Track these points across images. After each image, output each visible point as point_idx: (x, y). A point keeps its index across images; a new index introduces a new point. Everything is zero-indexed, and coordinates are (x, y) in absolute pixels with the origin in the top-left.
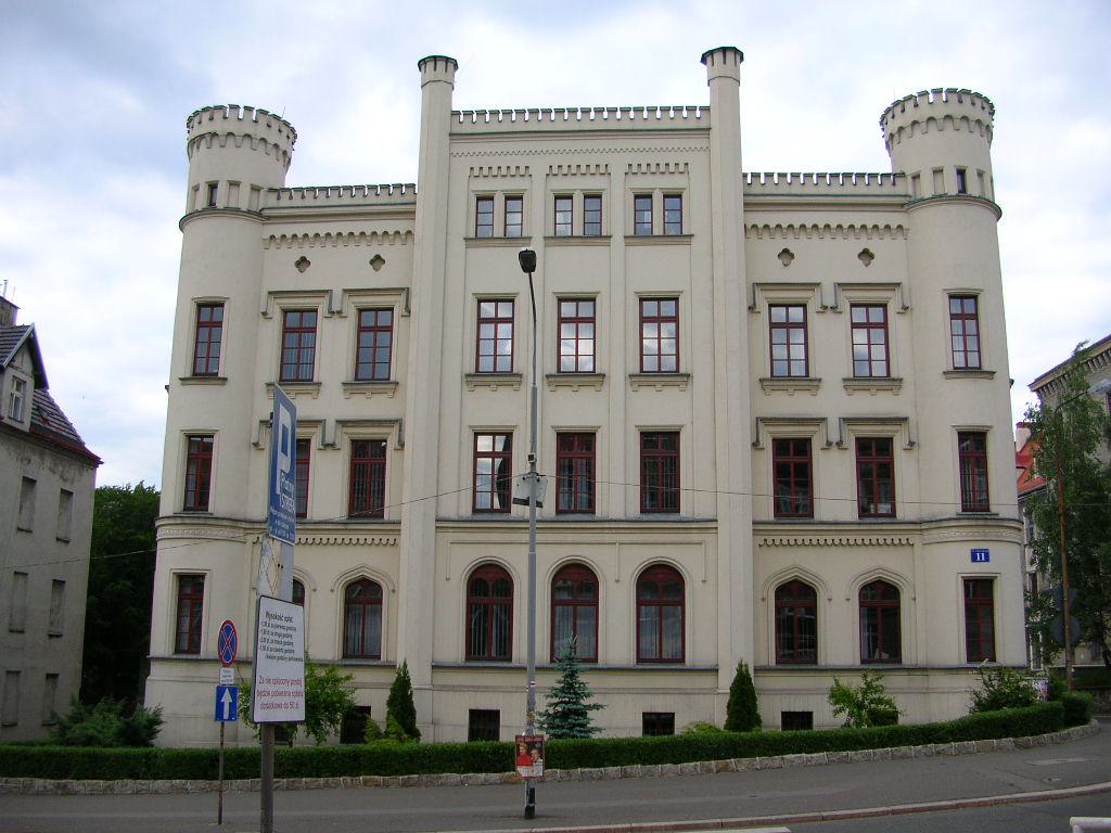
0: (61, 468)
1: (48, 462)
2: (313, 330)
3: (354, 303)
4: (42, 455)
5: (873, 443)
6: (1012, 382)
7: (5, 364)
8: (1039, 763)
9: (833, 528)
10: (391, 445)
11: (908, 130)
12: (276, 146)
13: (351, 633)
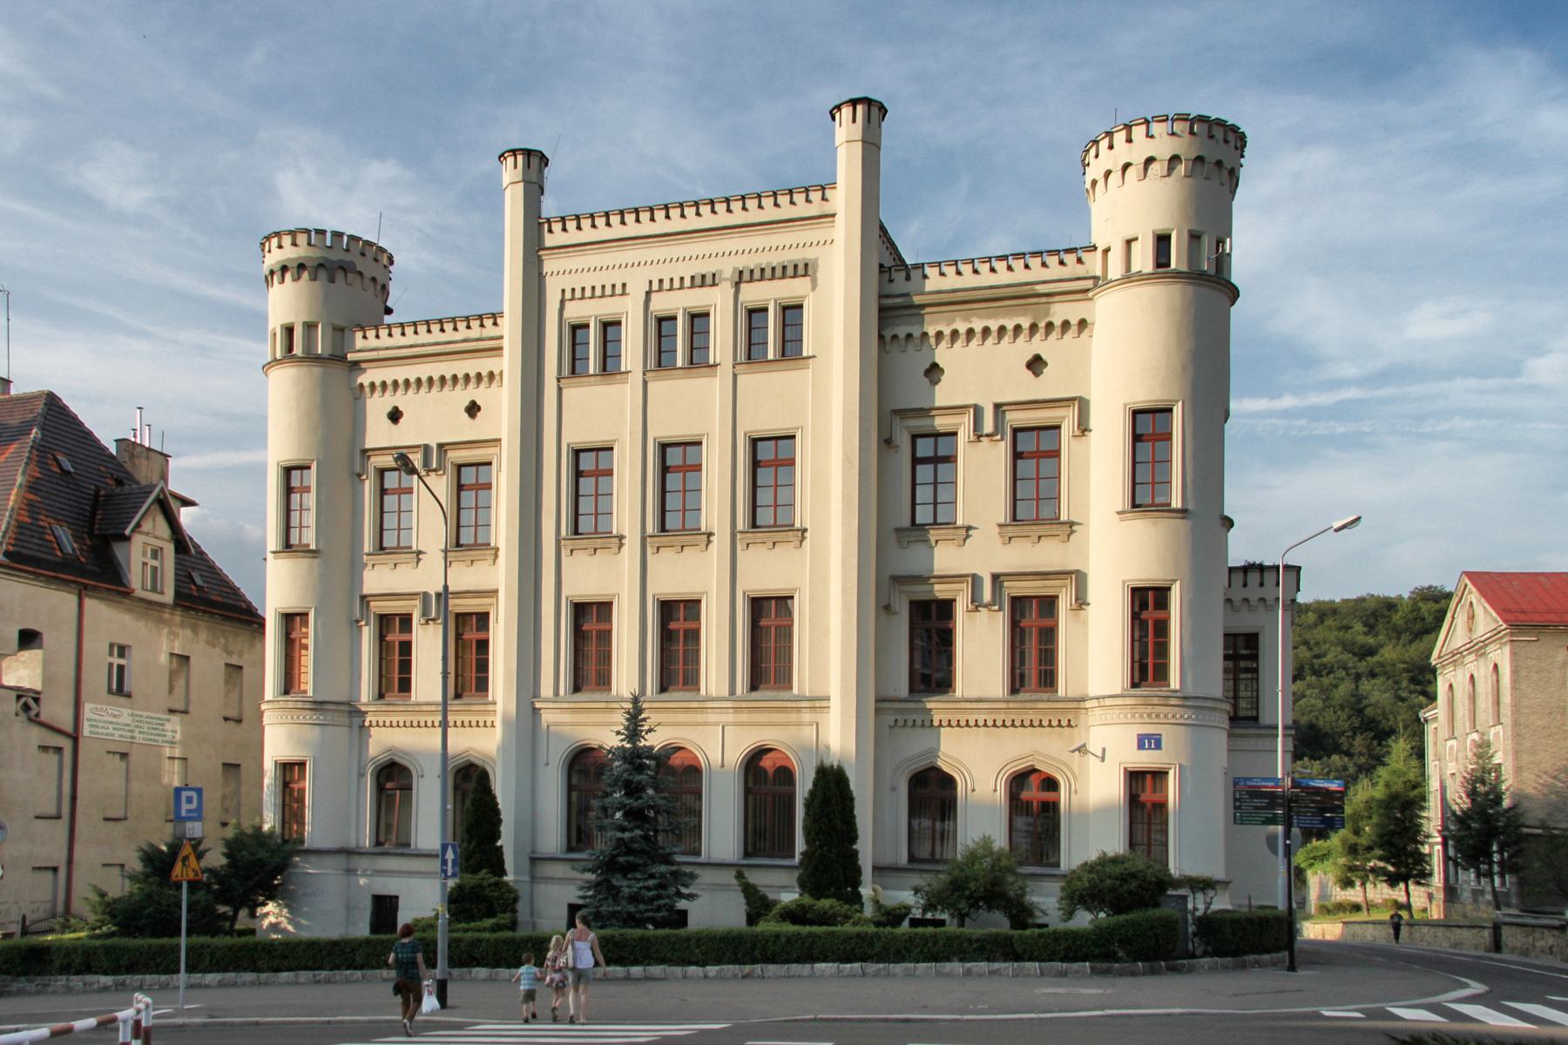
0: (222, 641)
1: (203, 635)
2: (1056, 454)
3: (907, 428)
4: (195, 629)
5: (934, 607)
7: (127, 532)
8: (1037, 991)
9: (975, 705)
10: (1064, 605)
12: (374, 280)
13: (916, 826)
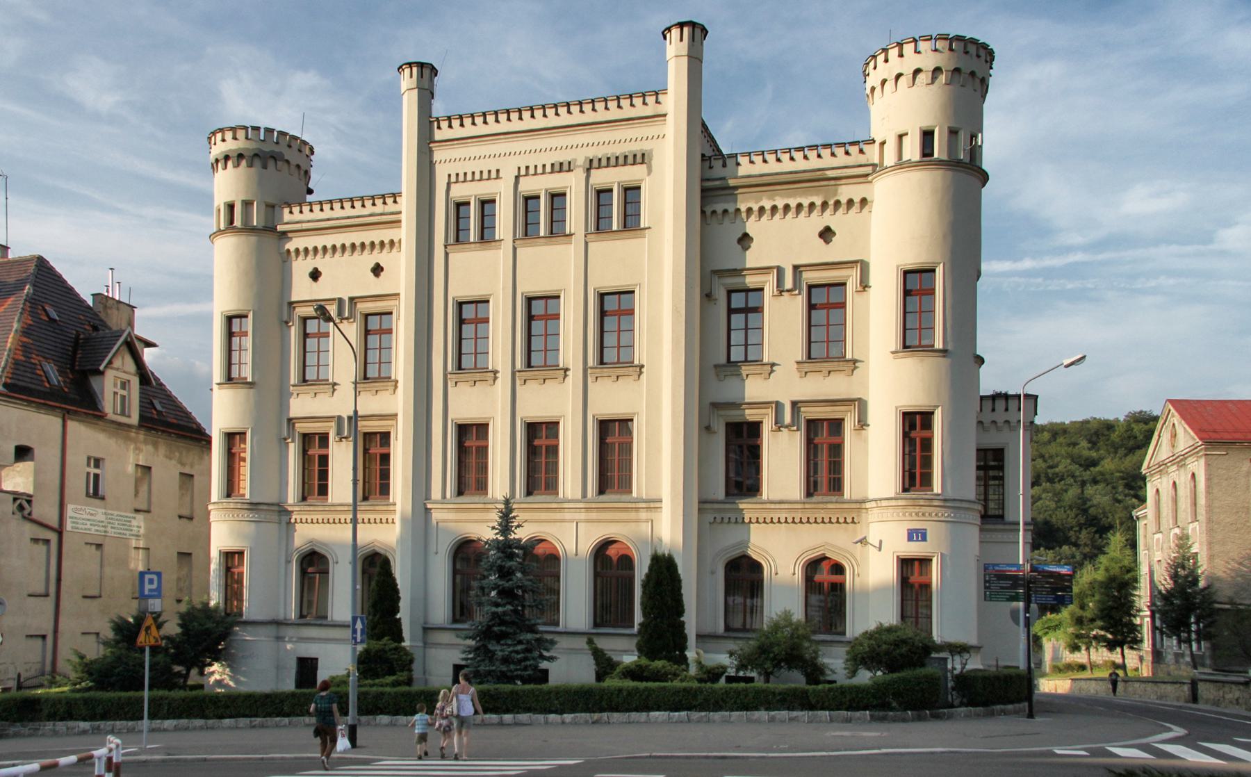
0: (177, 454)
1: (162, 450)
2: (842, 305)
3: (724, 285)
4: (155, 445)
6: (980, 361)
8: (828, 734)
9: (778, 506)
10: (849, 426)
11: (878, 89)
12: (298, 166)
